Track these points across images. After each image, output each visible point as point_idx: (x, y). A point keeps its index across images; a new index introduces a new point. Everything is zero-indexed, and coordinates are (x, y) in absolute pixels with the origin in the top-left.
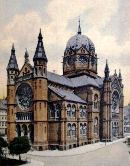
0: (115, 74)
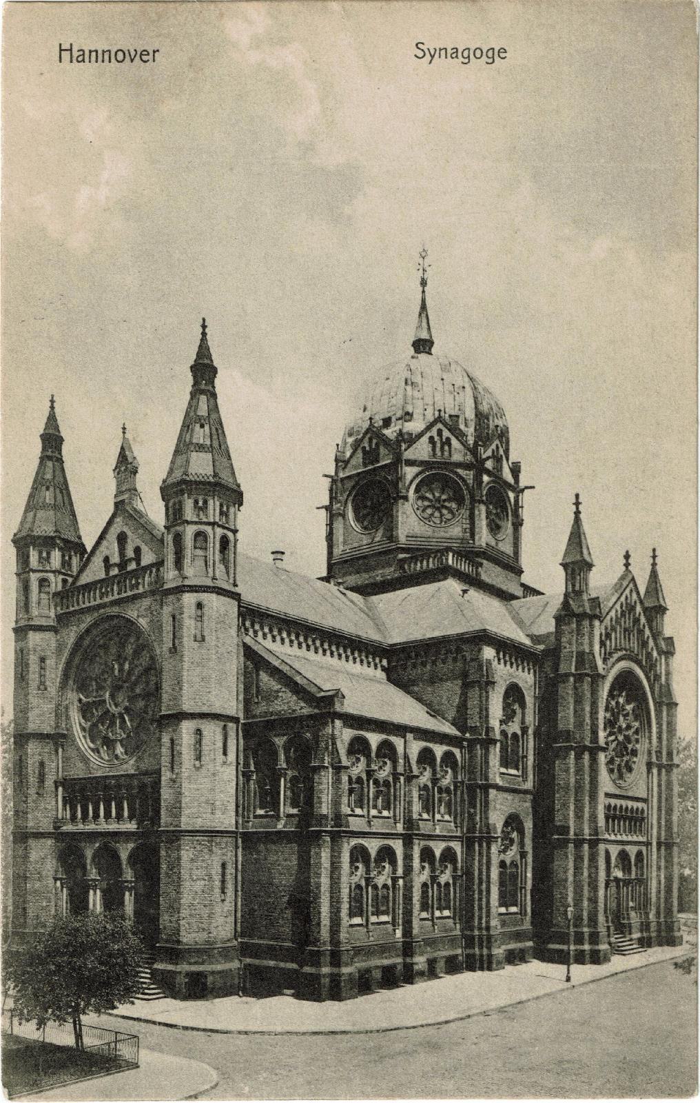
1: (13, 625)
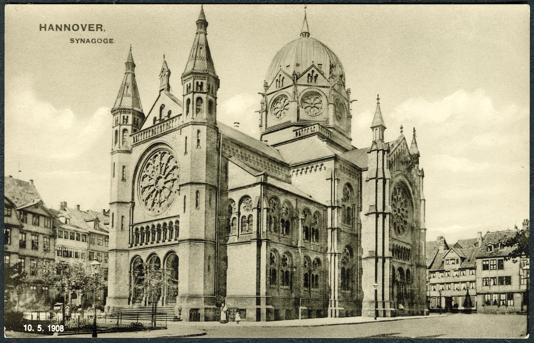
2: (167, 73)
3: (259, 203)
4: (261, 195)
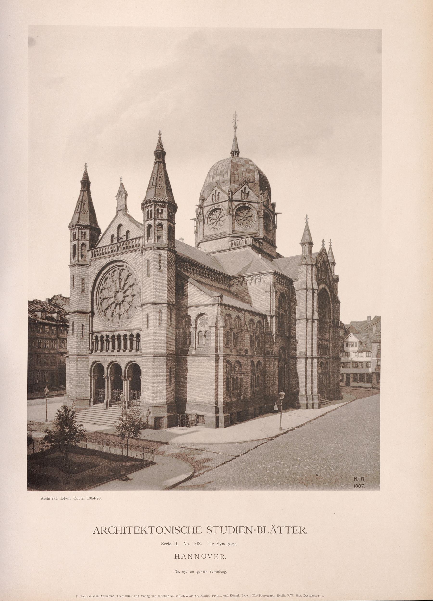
0: (323, 250)
1: (69, 264)
2: (124, 195)
3: (216, 322)
4: (218, 314)
